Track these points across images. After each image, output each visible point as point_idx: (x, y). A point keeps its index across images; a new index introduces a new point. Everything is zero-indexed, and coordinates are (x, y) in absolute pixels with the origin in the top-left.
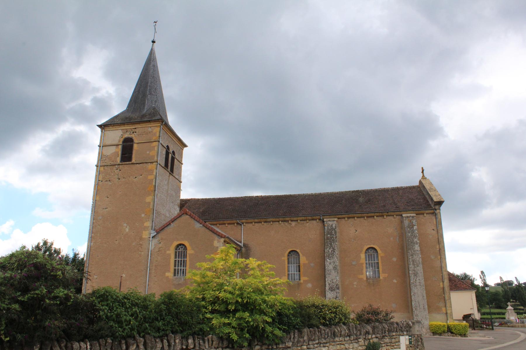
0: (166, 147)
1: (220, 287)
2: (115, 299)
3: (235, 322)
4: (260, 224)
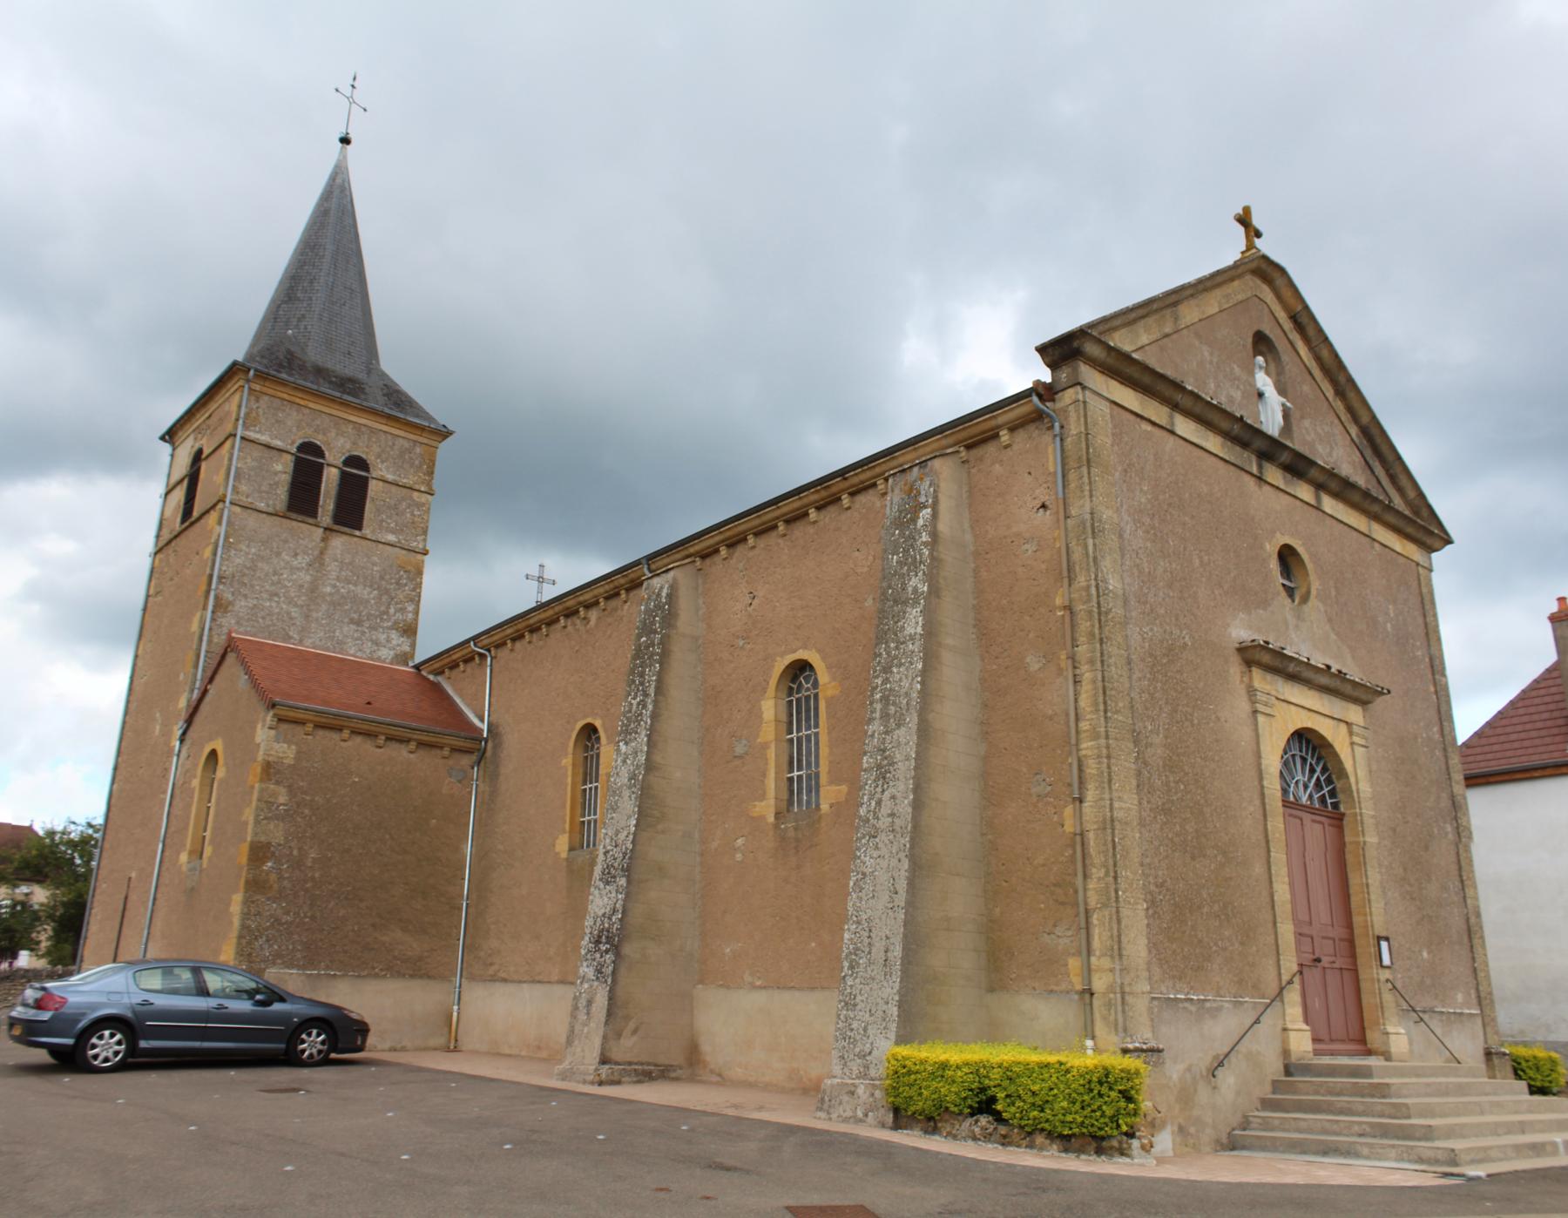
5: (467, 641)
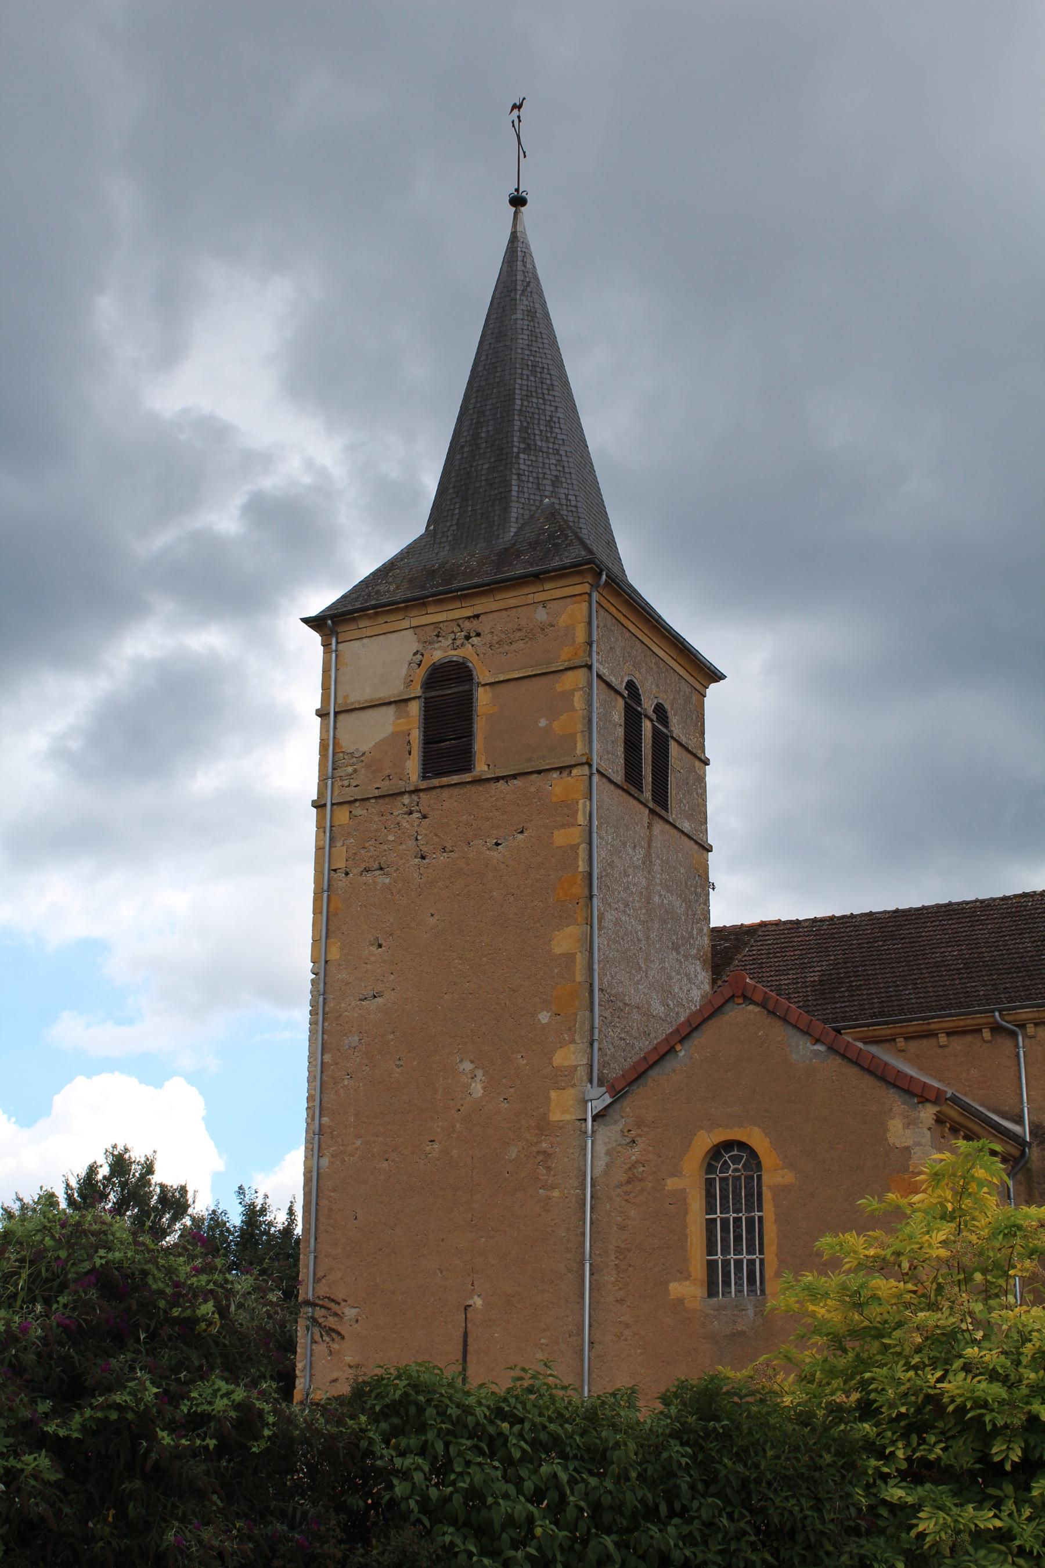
0: (622, 688)
1: (944, 1348)
2: (458, 1422)
3: (1029, 1528)
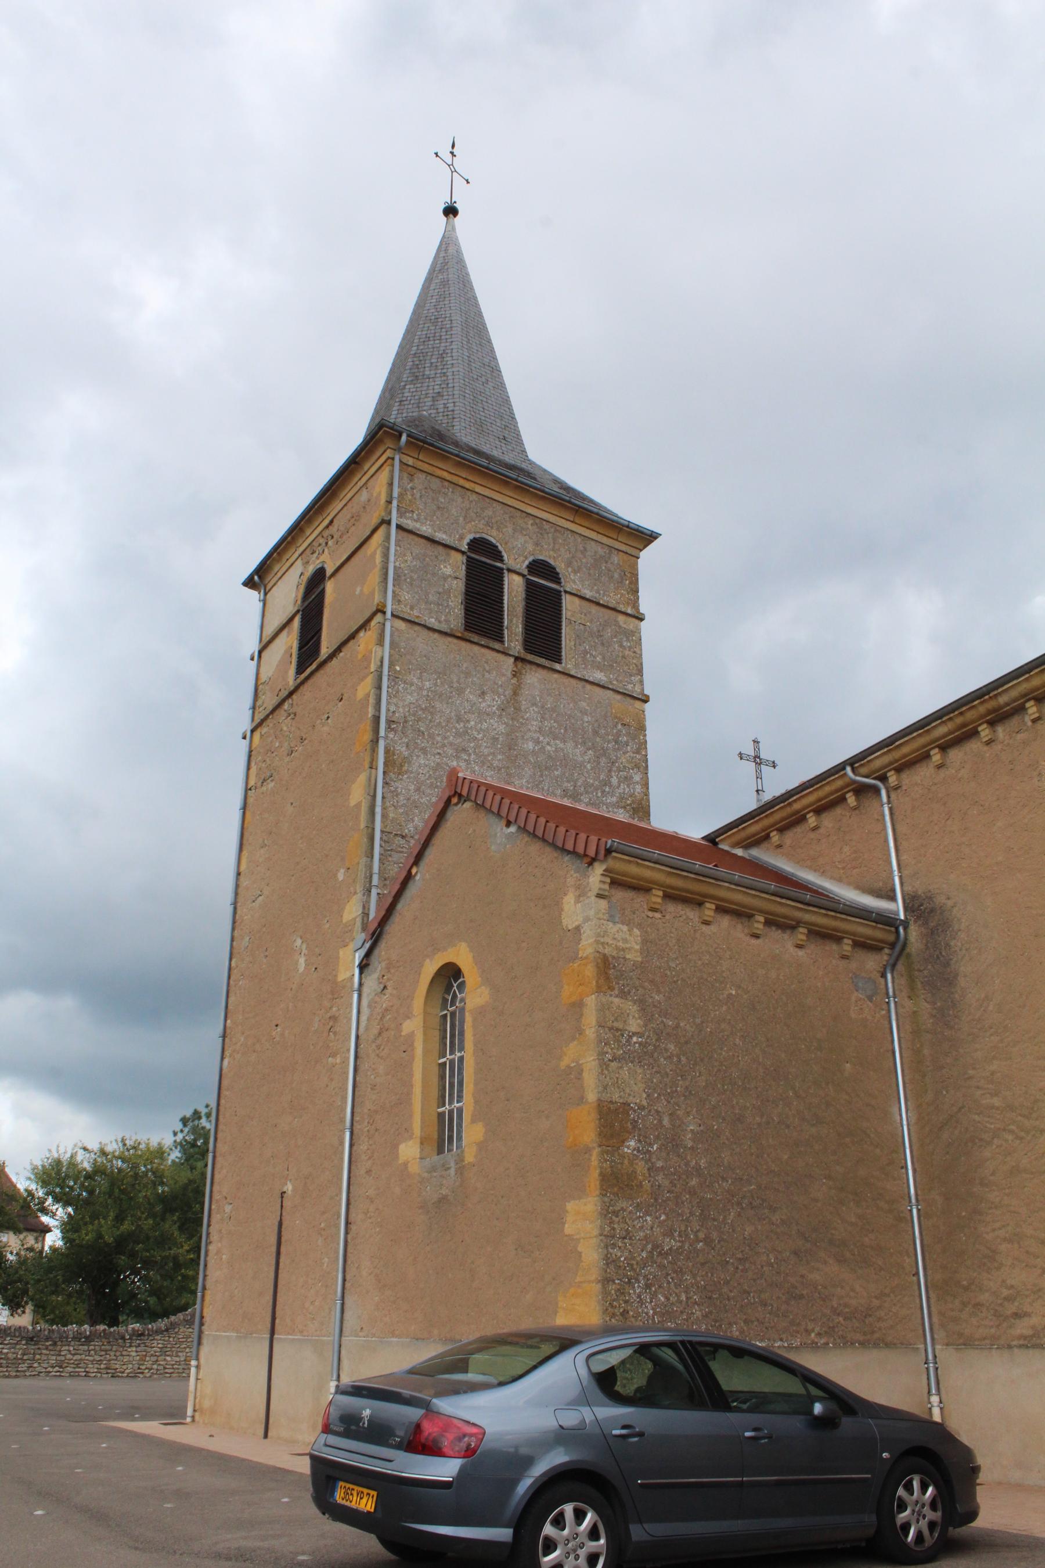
4: (973, 746)
5: (840, 768)
